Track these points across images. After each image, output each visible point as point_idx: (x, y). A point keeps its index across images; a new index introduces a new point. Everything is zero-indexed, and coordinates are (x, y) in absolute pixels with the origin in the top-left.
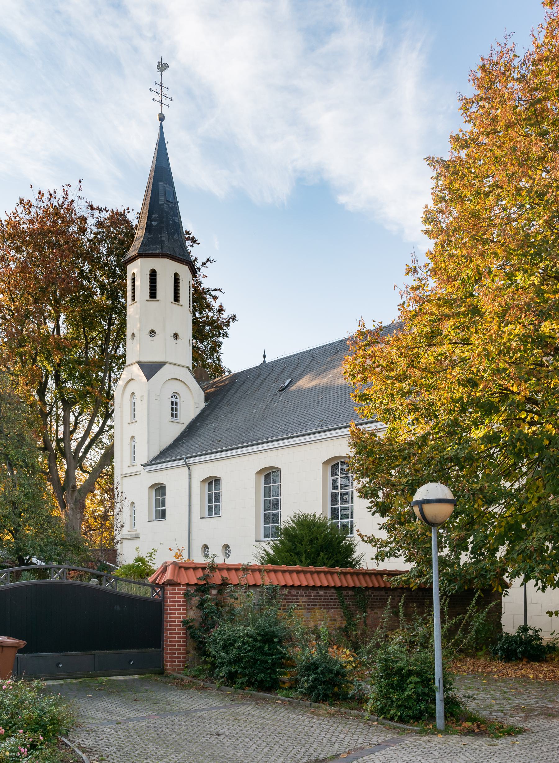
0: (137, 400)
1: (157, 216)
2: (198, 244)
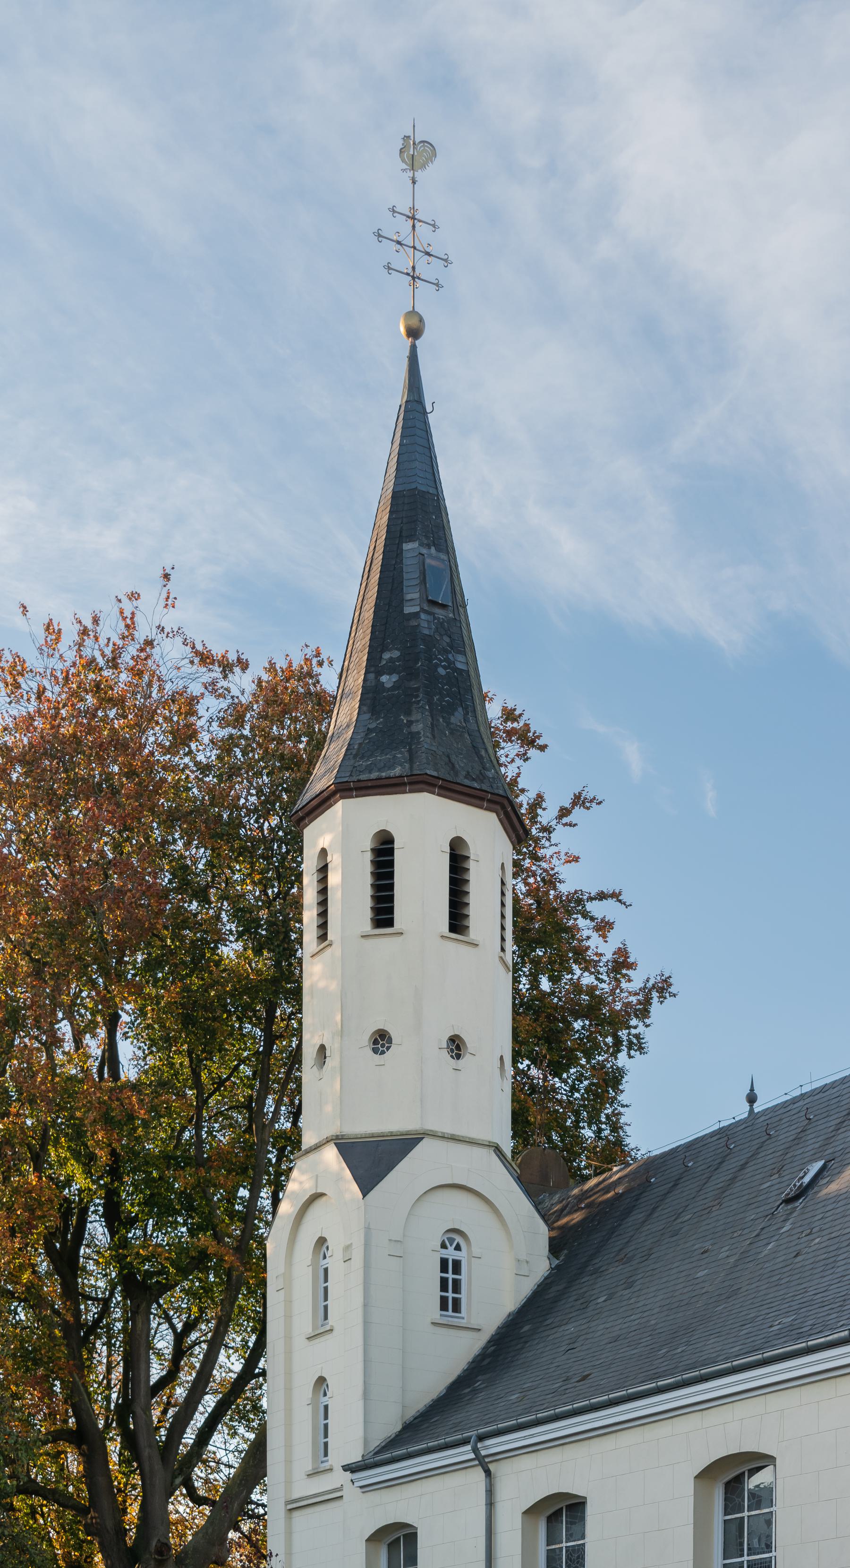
0: (334, 1263)
1: (396, 654)
2: (543, 748)
